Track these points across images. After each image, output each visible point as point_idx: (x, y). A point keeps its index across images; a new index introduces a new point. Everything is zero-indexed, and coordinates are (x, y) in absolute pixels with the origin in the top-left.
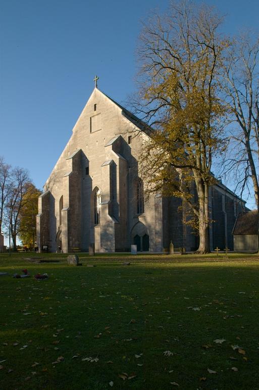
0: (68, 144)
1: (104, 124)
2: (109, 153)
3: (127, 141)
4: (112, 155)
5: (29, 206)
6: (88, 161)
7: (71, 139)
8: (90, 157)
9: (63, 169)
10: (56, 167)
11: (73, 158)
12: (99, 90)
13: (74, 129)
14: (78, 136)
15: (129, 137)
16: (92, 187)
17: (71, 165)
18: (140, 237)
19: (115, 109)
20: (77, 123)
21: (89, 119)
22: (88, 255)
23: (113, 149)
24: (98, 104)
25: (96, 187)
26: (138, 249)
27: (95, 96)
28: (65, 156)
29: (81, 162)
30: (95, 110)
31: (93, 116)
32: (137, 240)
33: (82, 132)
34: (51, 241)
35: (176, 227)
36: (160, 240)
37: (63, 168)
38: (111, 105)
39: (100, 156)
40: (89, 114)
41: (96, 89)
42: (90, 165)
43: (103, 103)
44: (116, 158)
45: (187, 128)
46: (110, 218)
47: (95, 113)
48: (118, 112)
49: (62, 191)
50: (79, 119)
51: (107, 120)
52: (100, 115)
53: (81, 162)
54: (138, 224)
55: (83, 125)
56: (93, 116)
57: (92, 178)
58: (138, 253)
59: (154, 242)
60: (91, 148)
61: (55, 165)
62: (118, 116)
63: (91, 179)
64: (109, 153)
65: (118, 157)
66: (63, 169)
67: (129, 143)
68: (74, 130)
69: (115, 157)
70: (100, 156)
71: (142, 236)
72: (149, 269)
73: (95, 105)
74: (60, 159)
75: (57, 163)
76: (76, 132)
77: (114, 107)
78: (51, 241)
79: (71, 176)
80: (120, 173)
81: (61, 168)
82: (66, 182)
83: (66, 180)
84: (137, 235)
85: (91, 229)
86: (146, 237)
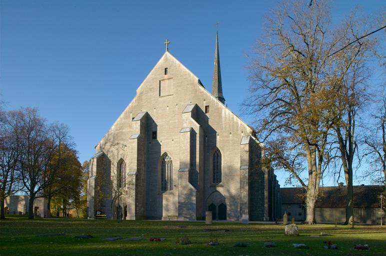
0: (130, 105)
1: (177, 90)
2: (187, 120)
3: (204, 111)
4: (192, 123)
5: (56, 169)
6: (156, 126)
7: (134, 100)
8: (159, 121)
9: (124, 131)
10: (113, 127)
11: (141, 120)
12: (171, 53)
13: (138, 89)
14: (144, 97)
15: (207, 107)
16: (160, 153)
17: (139, 128)
18: (216, 206)
19: (190, 76)
20: (142, 84)
21: (159, 82)
22: (204, 224)
23: (192, 117)
24: (170, 68)
25: (166, 153)
26: (214, 218)
27: (166, 60)
28: (126, 117)
29: (148, 127)
30: (166, 74)
31: (163, 80)
32: (212, 208)
33: (149, 94)
34: (104, 206)
35: (258, 199)
36: (247, 211)
37: (123, 129)
38: (186, 72)
39: (171, 122)
40: (158, 76)
41: (167, 53)
42: (158, 129)
43: (176, 69)
44: (197, 127)
45: (322, 110)
46: (191, 186)
47: (166, 77)
48: (194, 80)
49: (128, 154)
50: (145, 80)
51: (180, 86)
52: (172, 80)
53: (148, 127)
54: (215, 193)
55: (151, 87)
56: (163, 80)
57: (161, 144)
58: (213, 221)
59: (23, 198)
60: (160, 112)
61: (112, 124)
62: (193, 84)
63: (160, 144)
64: (187, 120)
65: (198, 126)
66: (124, 131)
67: (206, 113)
68: (139, 90)
69: (195, 125)
70: (171, 122)
71: (218, 205)
72: (349, 241)
73: (166, 69)
74: (119, 119)
75: (116, 123)
76: (141, 93)
77: (189, 74)
78: (104, 206)
79: (139, 139)
80: (196, 140)
81: (120, 129)
82: (134, 145)
83: (134, 142)
84: (212, 204)
85: (158, 196)
86: (223, 207)
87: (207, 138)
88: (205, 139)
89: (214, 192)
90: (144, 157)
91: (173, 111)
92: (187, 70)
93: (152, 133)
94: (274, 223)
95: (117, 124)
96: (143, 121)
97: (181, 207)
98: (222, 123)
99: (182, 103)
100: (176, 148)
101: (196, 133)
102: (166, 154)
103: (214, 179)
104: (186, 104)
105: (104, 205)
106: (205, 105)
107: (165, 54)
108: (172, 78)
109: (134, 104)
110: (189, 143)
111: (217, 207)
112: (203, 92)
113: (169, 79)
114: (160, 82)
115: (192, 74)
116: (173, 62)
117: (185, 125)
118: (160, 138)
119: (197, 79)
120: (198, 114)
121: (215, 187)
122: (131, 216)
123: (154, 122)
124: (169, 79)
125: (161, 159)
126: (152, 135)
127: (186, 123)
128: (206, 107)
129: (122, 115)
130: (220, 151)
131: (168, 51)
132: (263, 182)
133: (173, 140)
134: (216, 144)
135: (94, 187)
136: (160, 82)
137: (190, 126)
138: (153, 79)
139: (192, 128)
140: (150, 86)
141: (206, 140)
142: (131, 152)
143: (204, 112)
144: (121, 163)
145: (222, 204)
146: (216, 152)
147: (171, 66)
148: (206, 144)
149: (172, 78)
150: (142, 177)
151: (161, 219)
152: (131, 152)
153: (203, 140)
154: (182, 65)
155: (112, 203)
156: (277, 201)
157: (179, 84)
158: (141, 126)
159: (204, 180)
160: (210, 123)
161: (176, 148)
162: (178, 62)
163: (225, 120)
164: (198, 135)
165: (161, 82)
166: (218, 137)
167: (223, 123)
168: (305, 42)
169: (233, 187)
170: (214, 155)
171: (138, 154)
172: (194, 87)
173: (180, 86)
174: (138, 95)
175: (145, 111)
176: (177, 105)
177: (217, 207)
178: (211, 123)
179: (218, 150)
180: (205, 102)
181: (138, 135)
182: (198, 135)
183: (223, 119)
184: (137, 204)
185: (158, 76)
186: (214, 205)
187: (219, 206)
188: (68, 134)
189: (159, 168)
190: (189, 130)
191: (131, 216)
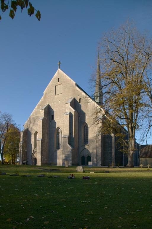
0: (40, 101)
2: (68, 107)
4: (70, 109)
5: (14, 140)
7: (42, 98)
8: (55, 109)
11: (44, 109)
12: (61, 70)
14: (47, 96)
15: (80, 99)
17: (44, 114)
19: (71, 82)
27: (59, 73)
28: (38, 108)
29: (49, 113)
30: (58, 82)
33: (50, 94)
39: (61, 109)
41: (59, 69)
44: (73, 111)
47: (58, 83)
48: (73, 84)
49: (38, 128)
50: (48, 86)
51: (66, 88)
52: (62, 85)
53: (49, 113)
54: (85, 150)
56: (57, 85)
62: (73, 86)
64: (68, 107)
65: (74, 110)
67: (80, 102)
68: (44, 92)
69: (72, 110)
70: (61, 109)
73: (58, 79)
74: (35, 109)
75: (33, 112)
76: (46, 94)
77: (71, 81)
82: (40, 123)
84: (83, 156)
87: (80, 118)
88: (79, 118)
89: (84, 149)
90: (47, 130)
91: (62, 103)
92: (70, 78)
93: (51, 116)
94: (107, 166)
95: (34, 112)
96: (46, 110)
97: (66, 159)
98: (88, 108)
99: (67, 98)
100: (62, 123)
101: (73, 115)
102: (59, 128)
103: (84, 142)
104: (69, 98)
105: (28, 157)
106: (79, 98)
107: (58, 70)
108: (62, 84)
109: (42, 100)
110: (68, 121)
111: (86, 158)
112: (78, 91)
113: (60, 84)
114: (55, 86)
115: (72, 81)
116: (62, 74)
117: (67, 111)
118: (56, 119)
119: (75, 83)
120: (75, 104)
121: (85, 146)
122: (39, 163)
123: (52, 109)
124: (60, 84)
125: (56, 131)
126: (51, 118)
127: (67, 109)
128: (80, 99)
129: (36, 107)
130: (87, 125)
131: (60, 68)
132: (111, 142)
133: (62, 120)
134: (85, 120)
135: (143, 144)
136: (55, 86)
137: (69, 111)
138: (52, 85)
139: (71, 112)
140: (50, 89)
141: (78, 118)
142: (39, 128)
143: (79, 102)
144: (36, 133)
145: (89, 156)
146: (85, 125)
147: (61, 77)
148: (80, 121)
149: (62, 84)
150: (46, 141)
151: (56, 165)
152: (39, 128)
153: (77, 118)
154: (67, 76)
155: (32, 156)
156: (140, 152)
157: (65, 87)
158: (45, 112)
159: (79, 142)
160: (82, 109)
161: (62, 123)
162: (65, 74)
163: (90, 106)
164: (74, 116)
165: (56, 86)
166: (86, 116)
167: (89, 108)
168: (120, 56)
169: (94, 147)
170: (84, 127)
171: (43, 129)
172: (73, 88)
173: (66, 88)
174: (44, 95)
175: (48, 104)
176: (64, 99)
177: (86, 158)
178: (83, 109)
179: (86, 124)
180: (79, 96)
181: (43, 118)
182: (74, 116)
183: (89, 106)
184: (42, 157)
185: (54, 84)
186: (84, 157)
187: (87, 157)
188: (12, 119)
189: (55, 136)
190: (68, 113)
191: (39, 163)
